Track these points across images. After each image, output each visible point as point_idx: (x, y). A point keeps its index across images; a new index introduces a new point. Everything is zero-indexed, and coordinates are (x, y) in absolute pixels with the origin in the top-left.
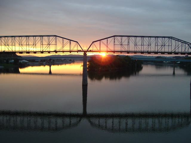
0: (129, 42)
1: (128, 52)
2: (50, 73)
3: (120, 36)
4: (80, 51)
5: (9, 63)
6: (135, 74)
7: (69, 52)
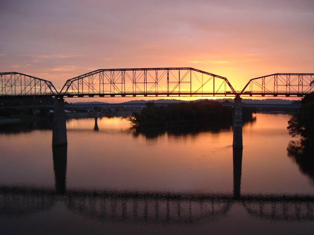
0: (145, 79)
2: (96, 128)
3: (177, 69)
5: (46, 112)
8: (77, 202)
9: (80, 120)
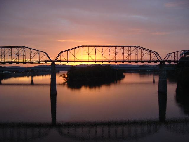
0: (109, 52)
1: (109, 62)
2: (32, 83)
3: (87, 46)
4: (49, 61)
6: (117, 82)
7: (102, 62)
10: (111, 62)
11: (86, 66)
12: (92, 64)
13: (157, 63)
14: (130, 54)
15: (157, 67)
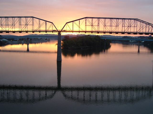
2: (28, 50)
4: (55, 31)
6: (105, 51)
7: (45, 32)
8: (67, 93)
9: (13, 45)
10: (106, 33)
11: (76, 36)
12: (81, 34)
13: (148, 35)
14: (111, 26)
15: (140, 38)
